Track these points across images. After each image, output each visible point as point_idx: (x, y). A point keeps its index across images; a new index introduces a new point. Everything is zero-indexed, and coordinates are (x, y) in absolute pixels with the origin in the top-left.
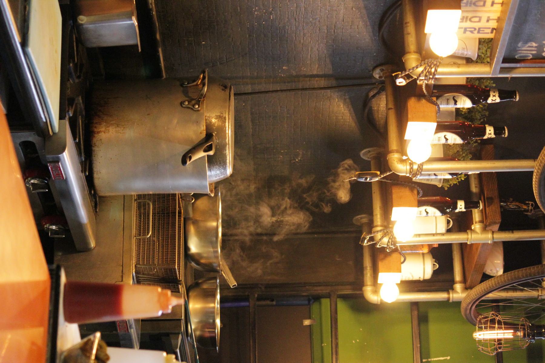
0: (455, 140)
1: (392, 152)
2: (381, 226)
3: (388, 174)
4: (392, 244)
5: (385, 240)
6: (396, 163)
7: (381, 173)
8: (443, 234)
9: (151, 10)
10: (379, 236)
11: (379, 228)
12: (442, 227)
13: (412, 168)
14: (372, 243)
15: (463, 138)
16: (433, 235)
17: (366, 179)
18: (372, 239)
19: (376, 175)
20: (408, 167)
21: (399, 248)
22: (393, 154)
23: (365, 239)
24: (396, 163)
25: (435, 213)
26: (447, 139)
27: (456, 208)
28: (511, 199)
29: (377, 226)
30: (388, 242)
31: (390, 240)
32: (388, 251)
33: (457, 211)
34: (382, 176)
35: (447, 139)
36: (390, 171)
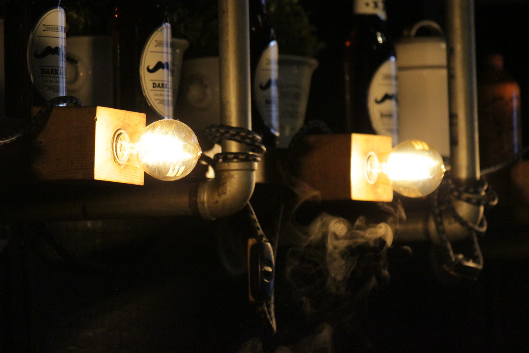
0: (160, 44)
1: (194, 204)
2: (426, 221)
3: (255, 217)
4: (477, 192)
5: (464, 209)
6: (224, 197)
7: (253, 233)
8: (450, 52)
9: (11, 141)
10: (452, 227)
11: (432, 226)
12: (434, 52)
13: (236, 156)
14: (477, 246)
15: (156, 25)
16: (451, 77)
17: (267, 274)
18: (463, 245)
19: (259, 247)
20: (235, 165)
21: (487, 171)
22: (200, 206)
23: (460, 267)
24: (224, 197)
25: (388, 77)
26: (160, 66)
27: (374, 18)
28: (254, 29)
29: (426, 231)
30: (468, 201)
31: (465, 196)
32: (495, 202)
33: (382, 15)
34: (261, 232)
35: (160, 66)
36: (246, 210)
